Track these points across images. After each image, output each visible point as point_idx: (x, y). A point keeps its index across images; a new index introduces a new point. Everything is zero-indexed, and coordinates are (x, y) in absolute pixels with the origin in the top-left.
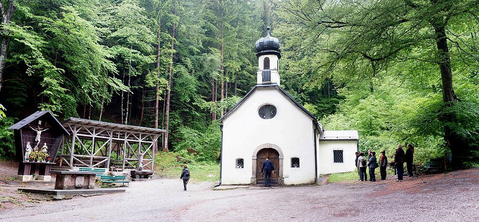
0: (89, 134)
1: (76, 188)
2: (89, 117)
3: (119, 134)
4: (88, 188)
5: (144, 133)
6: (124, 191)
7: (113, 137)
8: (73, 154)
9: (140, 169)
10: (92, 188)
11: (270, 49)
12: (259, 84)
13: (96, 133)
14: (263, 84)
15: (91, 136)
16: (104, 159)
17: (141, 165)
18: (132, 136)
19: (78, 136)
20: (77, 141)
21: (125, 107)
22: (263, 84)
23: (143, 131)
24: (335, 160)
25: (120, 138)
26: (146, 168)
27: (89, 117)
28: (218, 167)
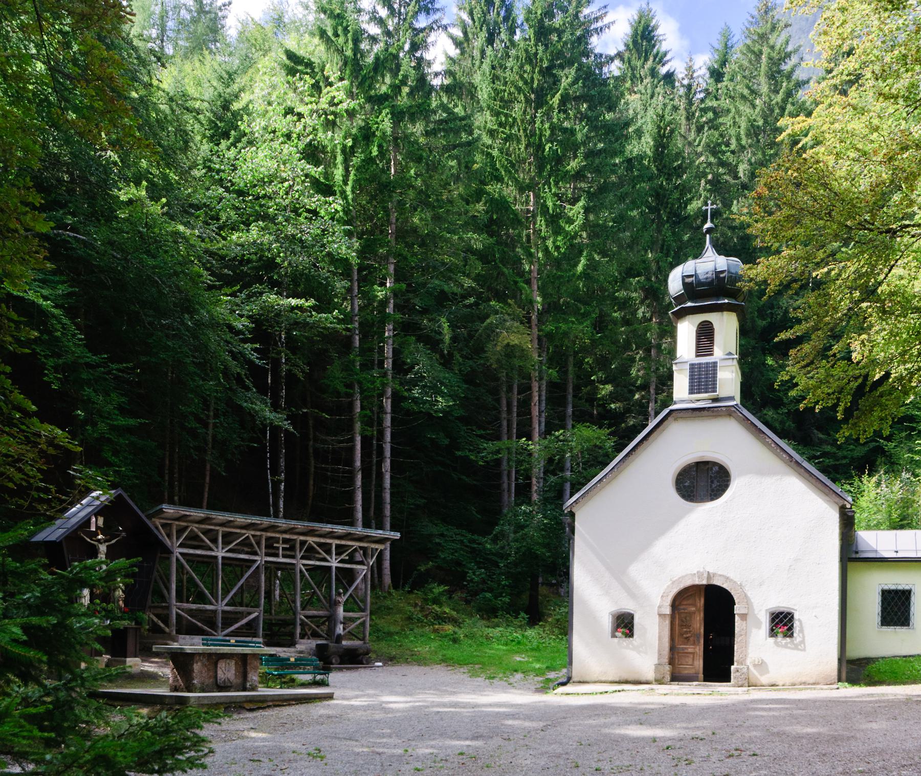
0: (211, 549)
1: (221, 688)
2: (176, 498)
3: (281, 546)
4: (245, 689)
5: (343, 542)
6: (330, 697)
7: (267, 555)
8: (174, 601)
9: (339, 638)
10: (253, 689)
11: (718, 296)
12: (682, 401)
13: (226, 543)
14: (691, 401)
15: (213, 554)
16: (249, 614)
17: (340, 630)
18: (194, 537)
19: (181, 554)
20: (306, 585)
21: (275, 472)
22: (691, 401)
23: (340, 537)
24: (882, 622)
25: (284, 556)
26: (351, 635)
27: (176, 498)
28: (562, 646)
